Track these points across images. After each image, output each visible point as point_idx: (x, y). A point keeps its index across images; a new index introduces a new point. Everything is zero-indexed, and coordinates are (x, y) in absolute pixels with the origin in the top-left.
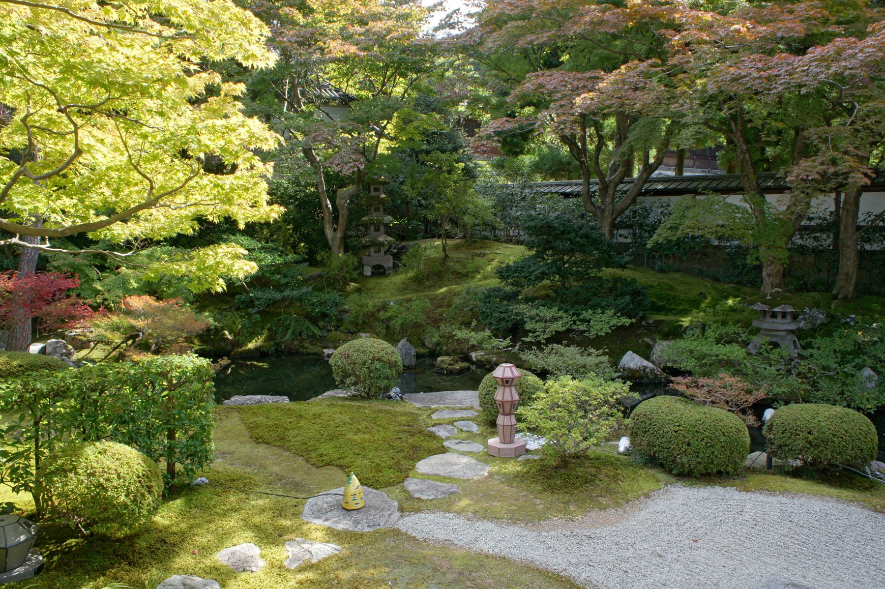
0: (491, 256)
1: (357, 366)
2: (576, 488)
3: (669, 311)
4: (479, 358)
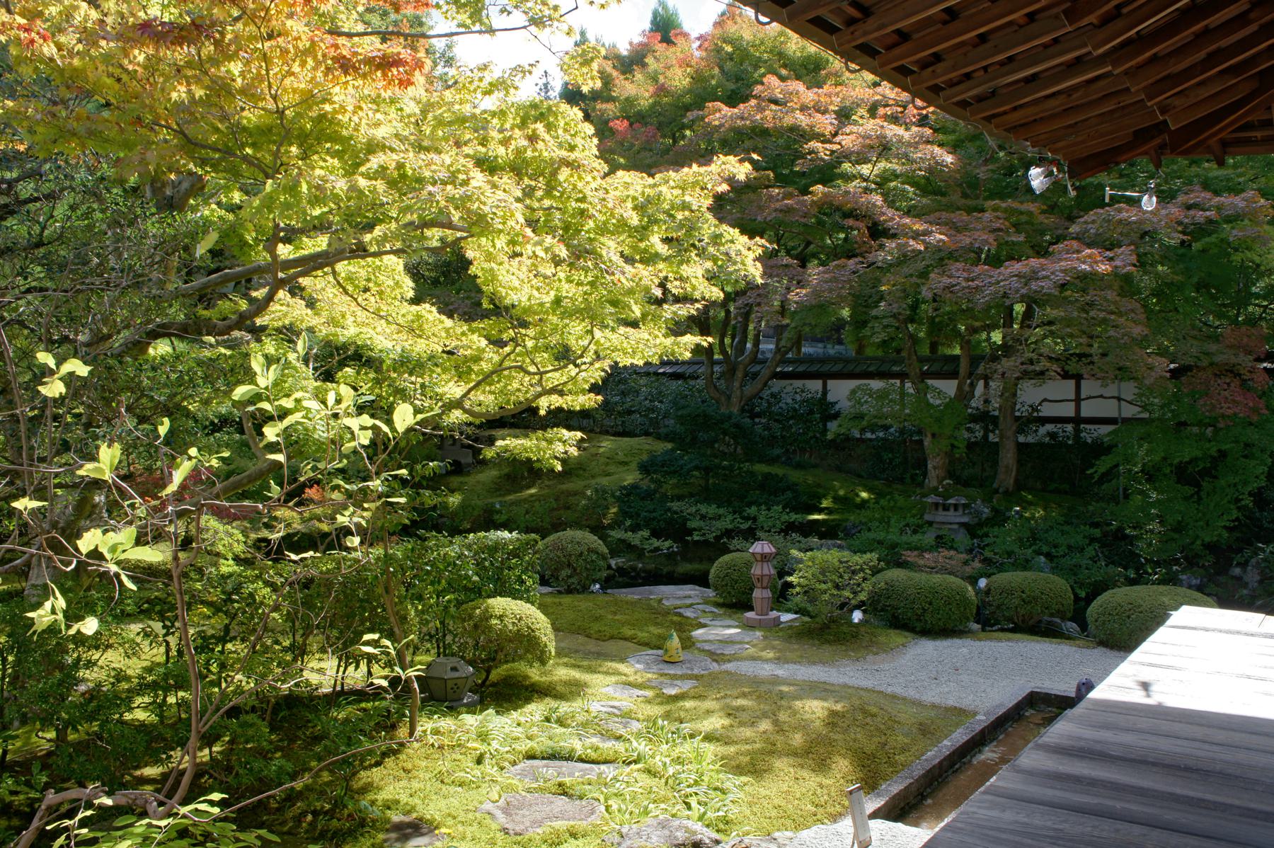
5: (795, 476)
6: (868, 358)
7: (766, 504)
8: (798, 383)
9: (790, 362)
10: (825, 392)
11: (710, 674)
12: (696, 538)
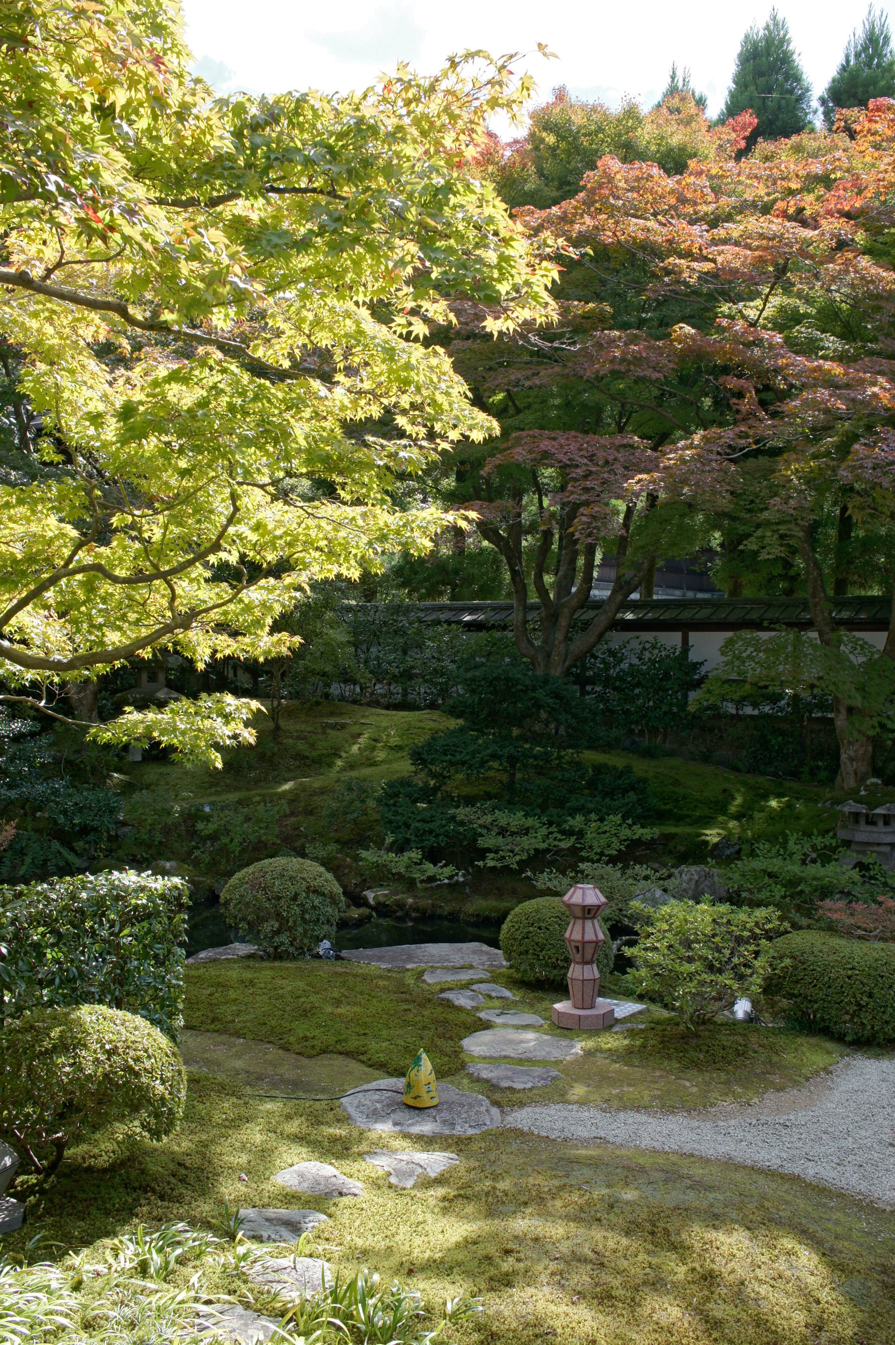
0: (355, 729)
1: (282, 902)
2: (729, 1063)
3: (679, 820)
4: (382, 899)
5: (641, 767)
6: (747, 601)
7: (596, 811)
8: (647, 636)
9: (634, 606)
10: (686, 646)
11: (485, 1136)
12: (491, 863)
